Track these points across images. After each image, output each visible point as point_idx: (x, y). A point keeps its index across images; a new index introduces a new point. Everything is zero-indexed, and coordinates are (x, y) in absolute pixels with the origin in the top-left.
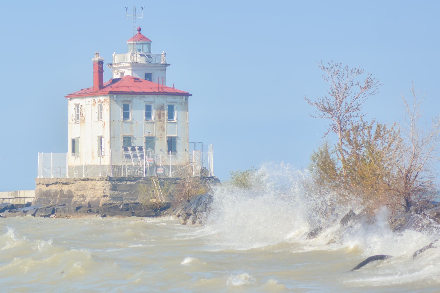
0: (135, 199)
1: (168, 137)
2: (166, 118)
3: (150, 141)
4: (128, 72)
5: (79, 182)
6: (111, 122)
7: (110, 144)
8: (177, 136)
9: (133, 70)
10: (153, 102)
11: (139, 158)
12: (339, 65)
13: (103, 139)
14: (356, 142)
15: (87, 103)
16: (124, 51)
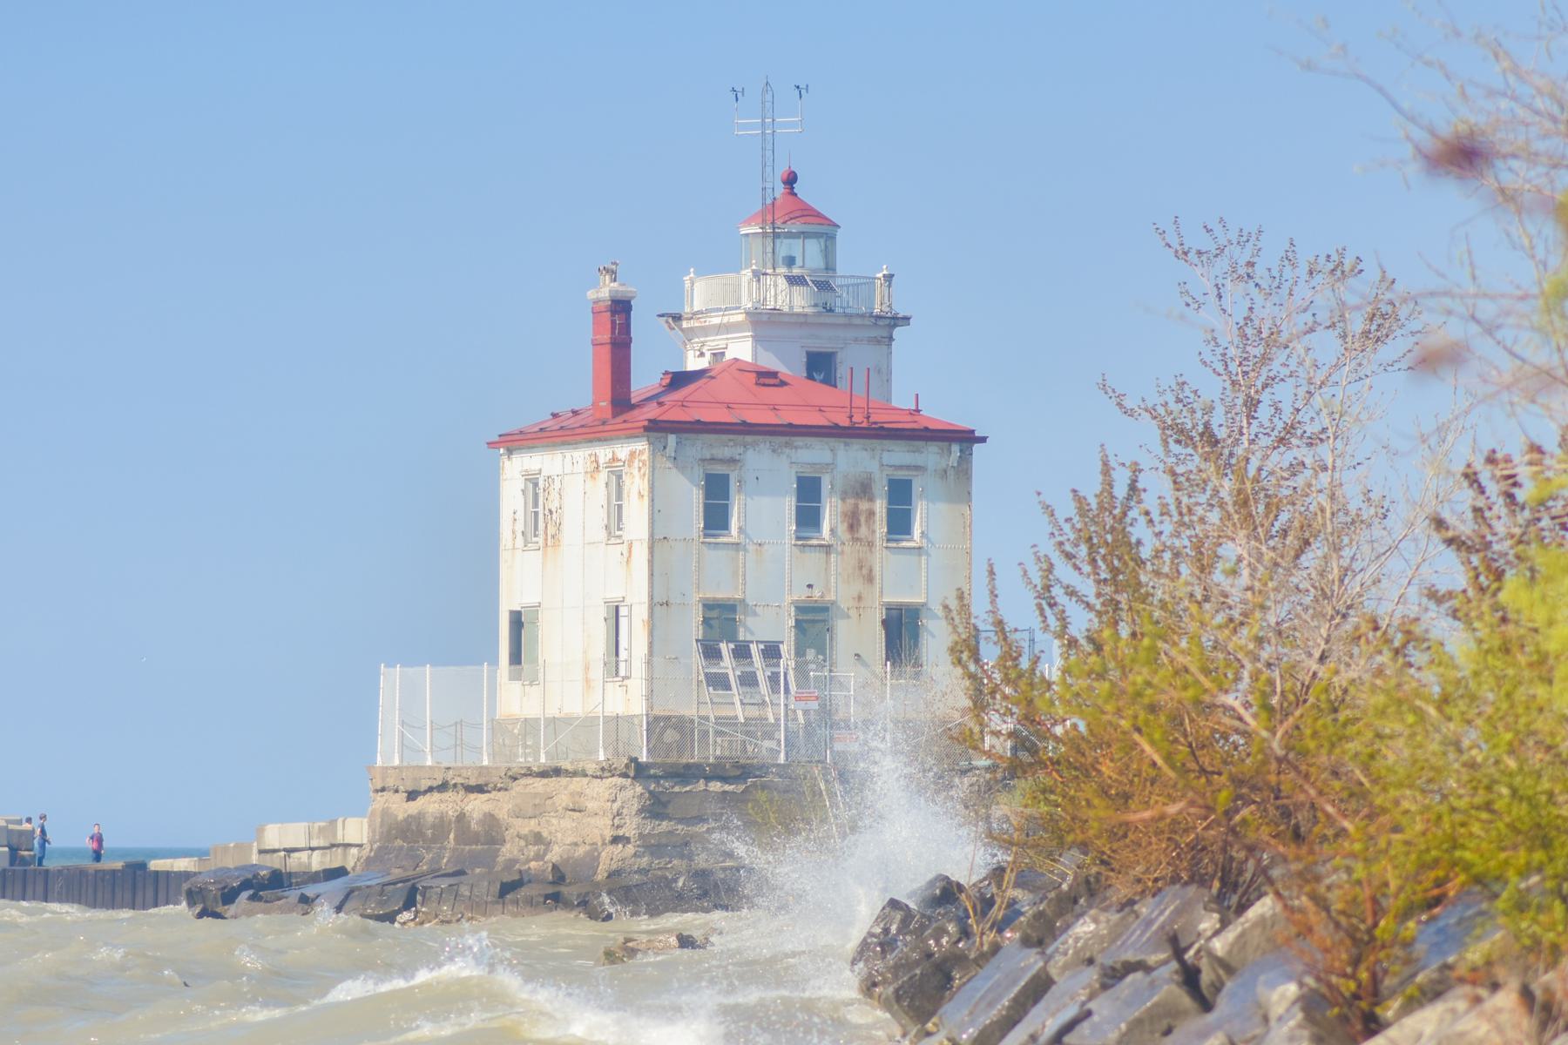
1: (889, 608)
2: (881, 528)
3: (814, 622)
4: (741, 349)
5: (523, 781)
6: (655, 542)
7: (651, 633)
8: (924, 605)
9: (757, 339)
10: (830, 467)
11: (764, 687)
12: (1254, 237)
13: (623, 611)
15: (568, 469)
16: (719, 263)
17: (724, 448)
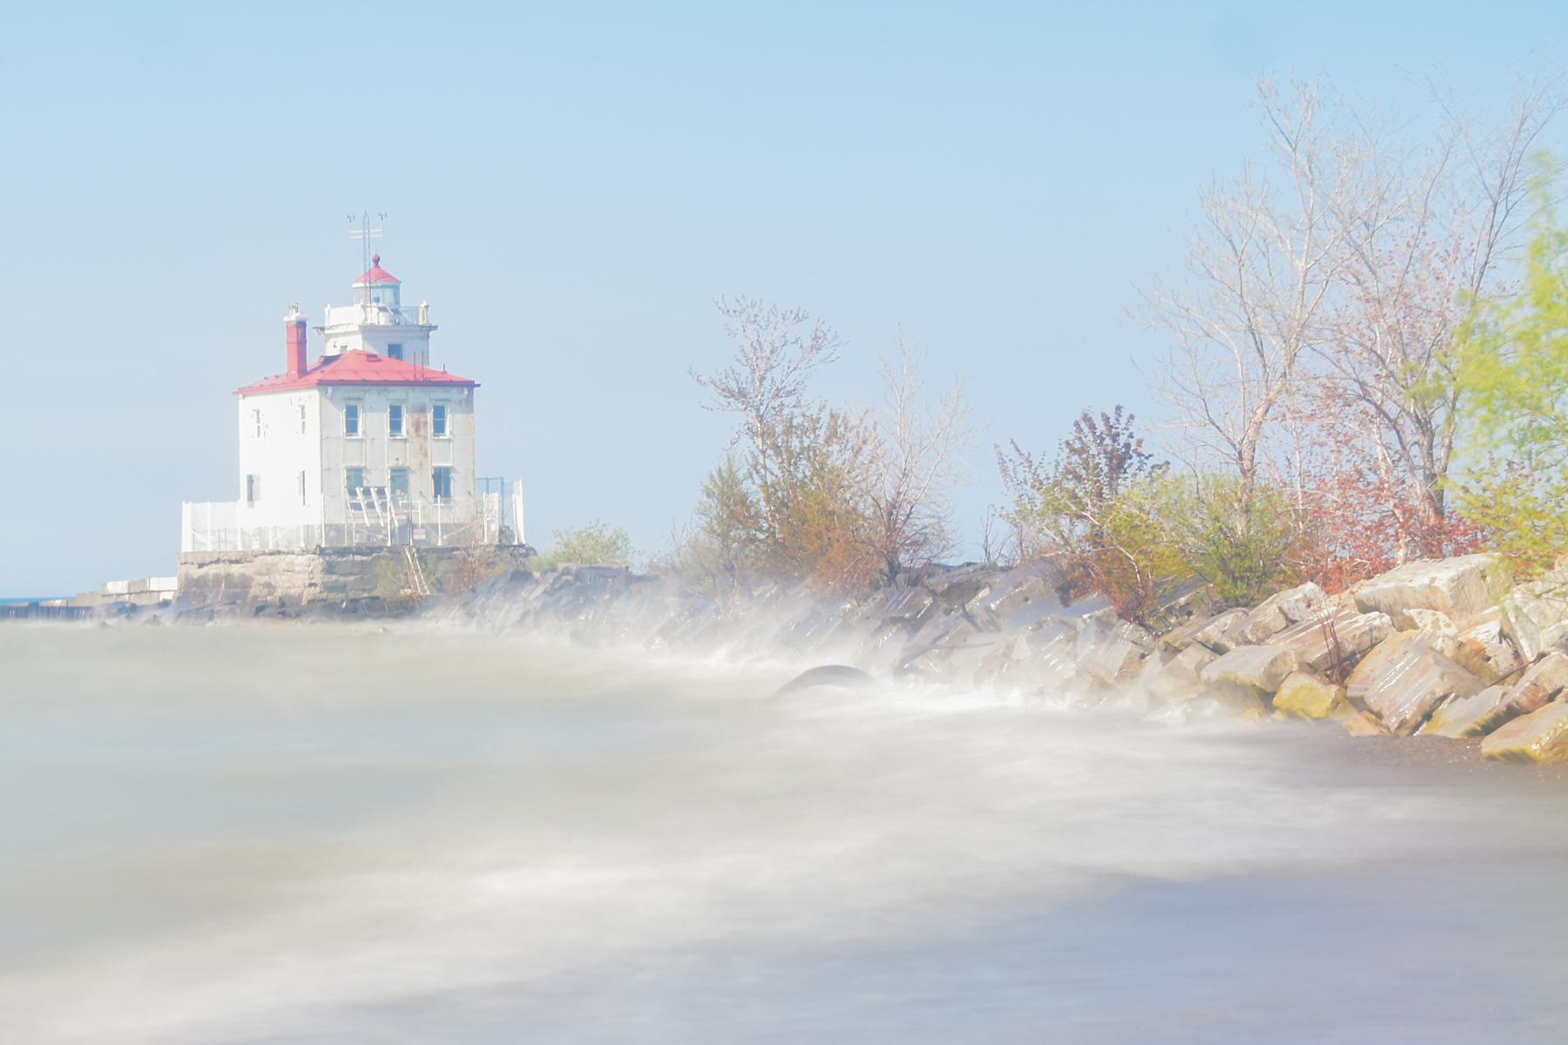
0: (371, 590)
2: (431, 430)
4: (356, 343)
14: (788, 449)
17: (355, 392)
